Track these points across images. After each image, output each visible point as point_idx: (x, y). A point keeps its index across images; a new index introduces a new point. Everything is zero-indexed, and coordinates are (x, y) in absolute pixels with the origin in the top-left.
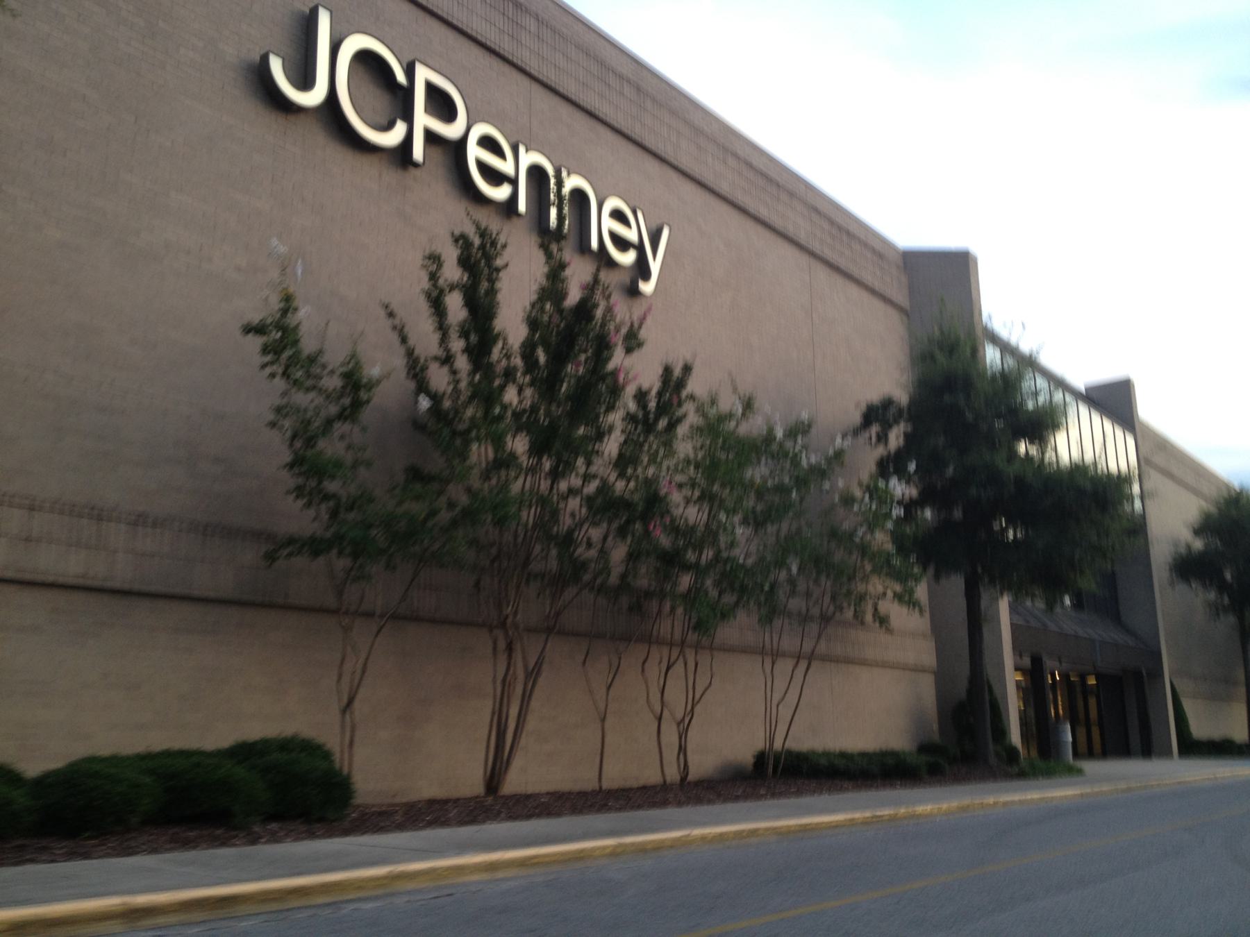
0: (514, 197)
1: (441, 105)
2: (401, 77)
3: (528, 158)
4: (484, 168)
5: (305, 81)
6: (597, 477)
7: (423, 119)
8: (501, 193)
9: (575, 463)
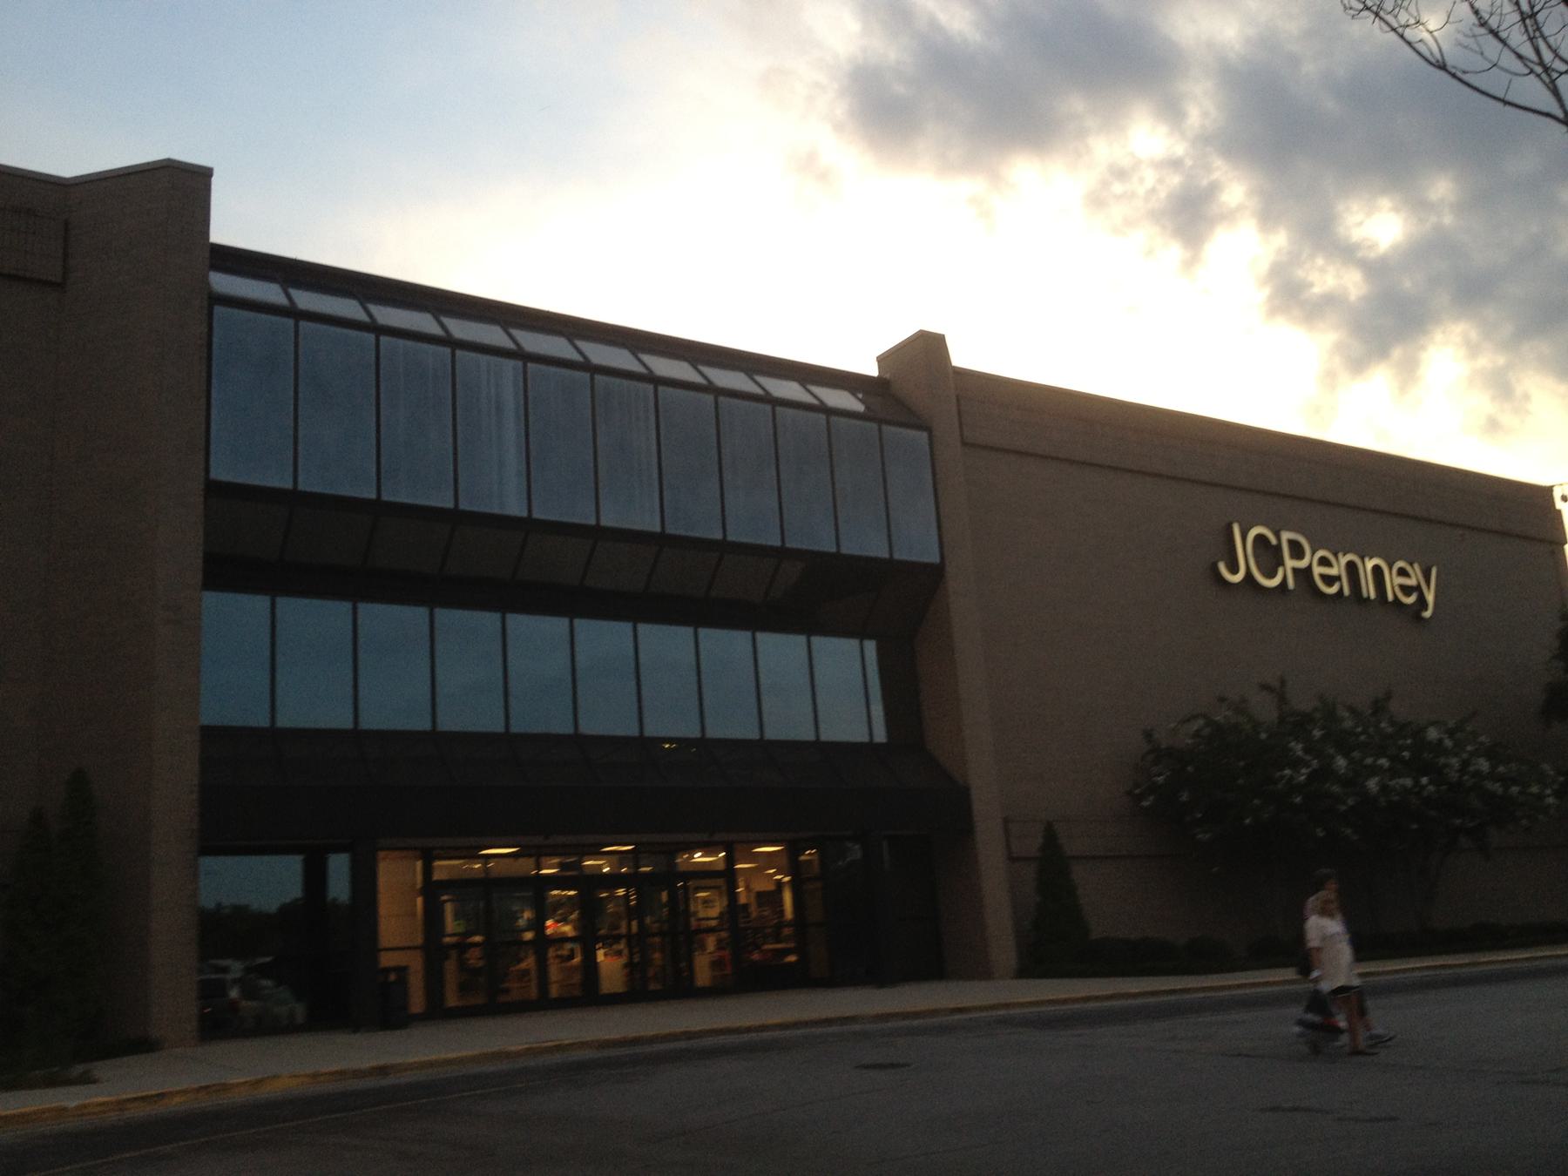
0: (1341, 590)
1: (1297, 551)
2: (1274, 541)
3: (1344, 560)
4: (1324, 577)
5: (1234, 569)
6: (1368, 1030)
7: (1290, 563)
8: (1333, 590)
9: (1358, 987)
